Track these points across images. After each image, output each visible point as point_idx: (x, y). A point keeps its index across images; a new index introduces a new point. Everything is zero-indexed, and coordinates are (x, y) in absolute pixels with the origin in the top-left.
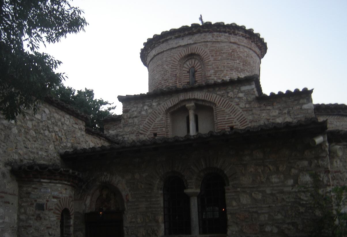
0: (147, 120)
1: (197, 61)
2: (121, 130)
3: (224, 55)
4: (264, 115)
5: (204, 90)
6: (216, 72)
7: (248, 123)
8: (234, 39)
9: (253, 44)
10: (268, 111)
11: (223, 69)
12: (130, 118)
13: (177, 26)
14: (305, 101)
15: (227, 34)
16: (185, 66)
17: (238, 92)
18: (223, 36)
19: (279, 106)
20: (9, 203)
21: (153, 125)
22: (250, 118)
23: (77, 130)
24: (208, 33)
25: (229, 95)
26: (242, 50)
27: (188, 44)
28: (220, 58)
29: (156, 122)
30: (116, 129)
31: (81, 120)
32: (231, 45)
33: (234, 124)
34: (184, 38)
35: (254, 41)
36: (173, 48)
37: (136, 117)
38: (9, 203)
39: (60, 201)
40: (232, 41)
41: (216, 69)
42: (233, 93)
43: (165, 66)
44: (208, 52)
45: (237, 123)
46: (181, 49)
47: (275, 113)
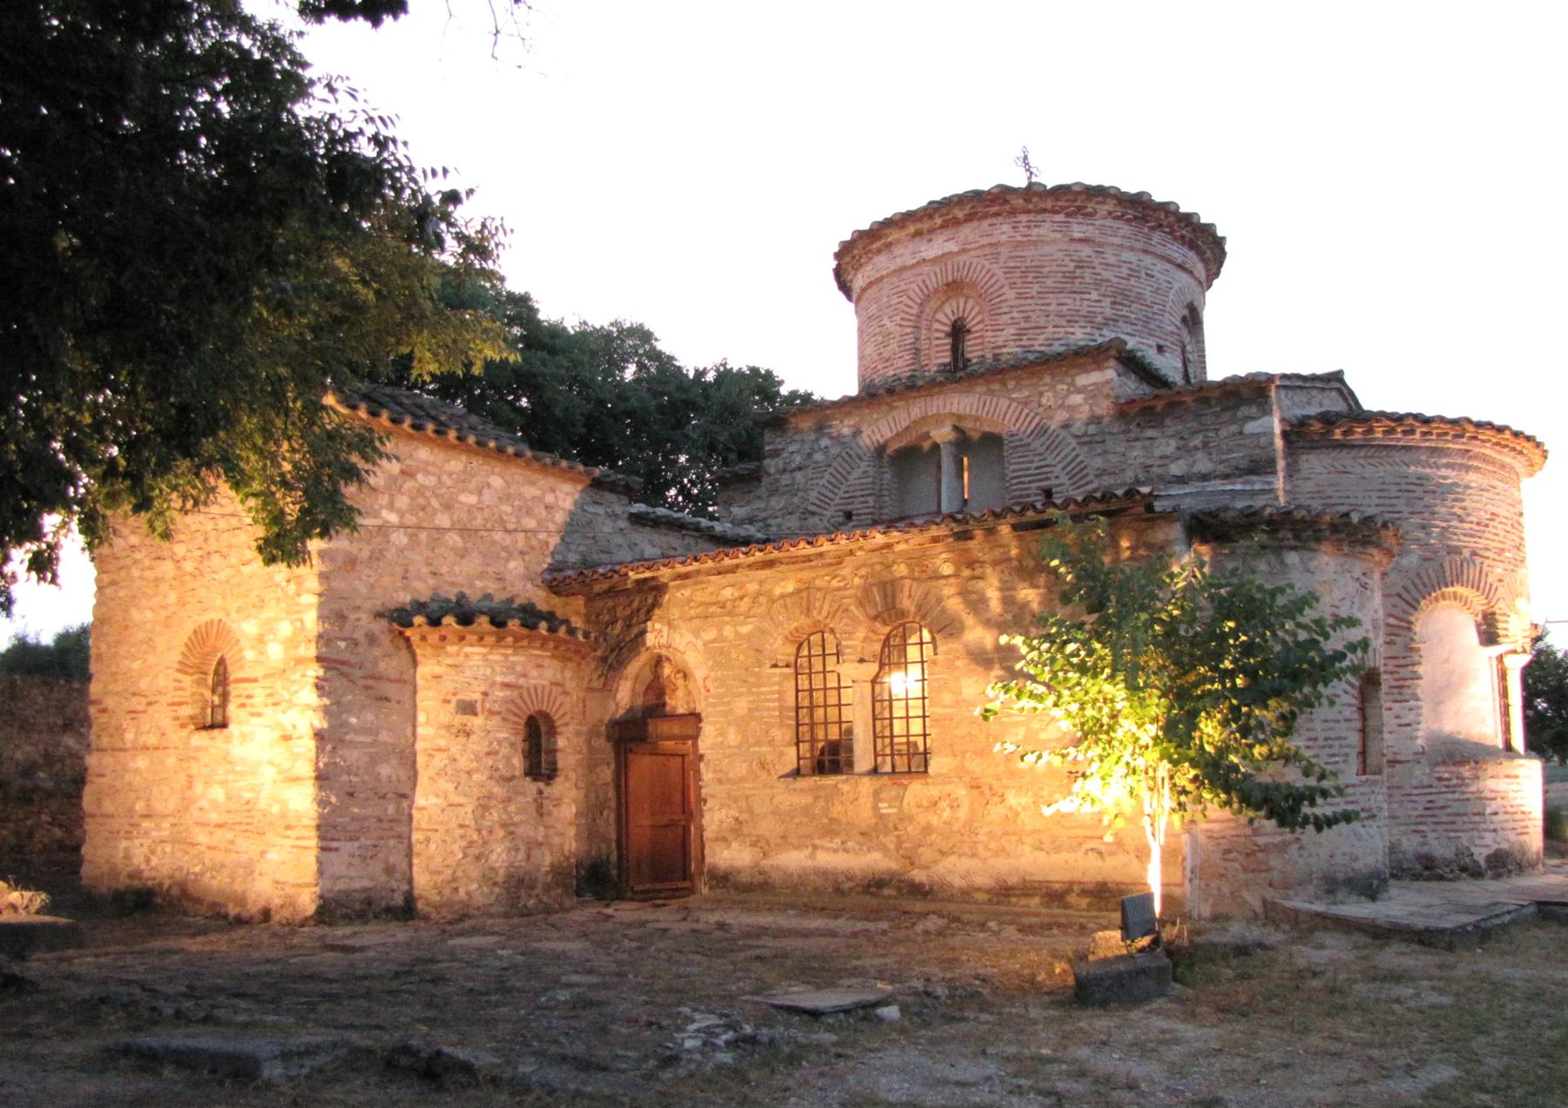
0: (827, 476)
1: (971, 303)
2: (762, 505)
3: (1049, 282)
4: (1137, 453)
5: (978, 389)
6: (1019, 335)
7: (1091, 477)
8: (1085, 228)
9: (1157, 237)
10: (1148, 443)
11: (1042, 321)
12: (784, 470)
13: (985, 185)
14: (1254, 410)
15: (1060, 217)
16: (940, 316)
17: (1069, 392)
18: (1047, 225)
19: (1179, 427)
20: (387, 699)
21: (843, 488)
22: (1098, 462)
23: (600, 519)
24: (1000, 219)
25: (1044, 401)
26: (1112, 260)
27: (943, 255)
28: (1036, 288)
29: (852, 481)
30: (748, 503)
31: (612, 491)
32: (1078, 246)
33: (1053, 482)
34: (934, 237)
35: (1160, 226)
36: (904, 269)
37: (800, 469)
38: (387, 699)
39: (521, 696)
40: (1077, 235)
41: (1023, 325)
42: (1056, 393)
43: (886, 321)
44: (1000, 274)
45: (1064, 479)
46: (926, 269)
47: (1168, 446)
